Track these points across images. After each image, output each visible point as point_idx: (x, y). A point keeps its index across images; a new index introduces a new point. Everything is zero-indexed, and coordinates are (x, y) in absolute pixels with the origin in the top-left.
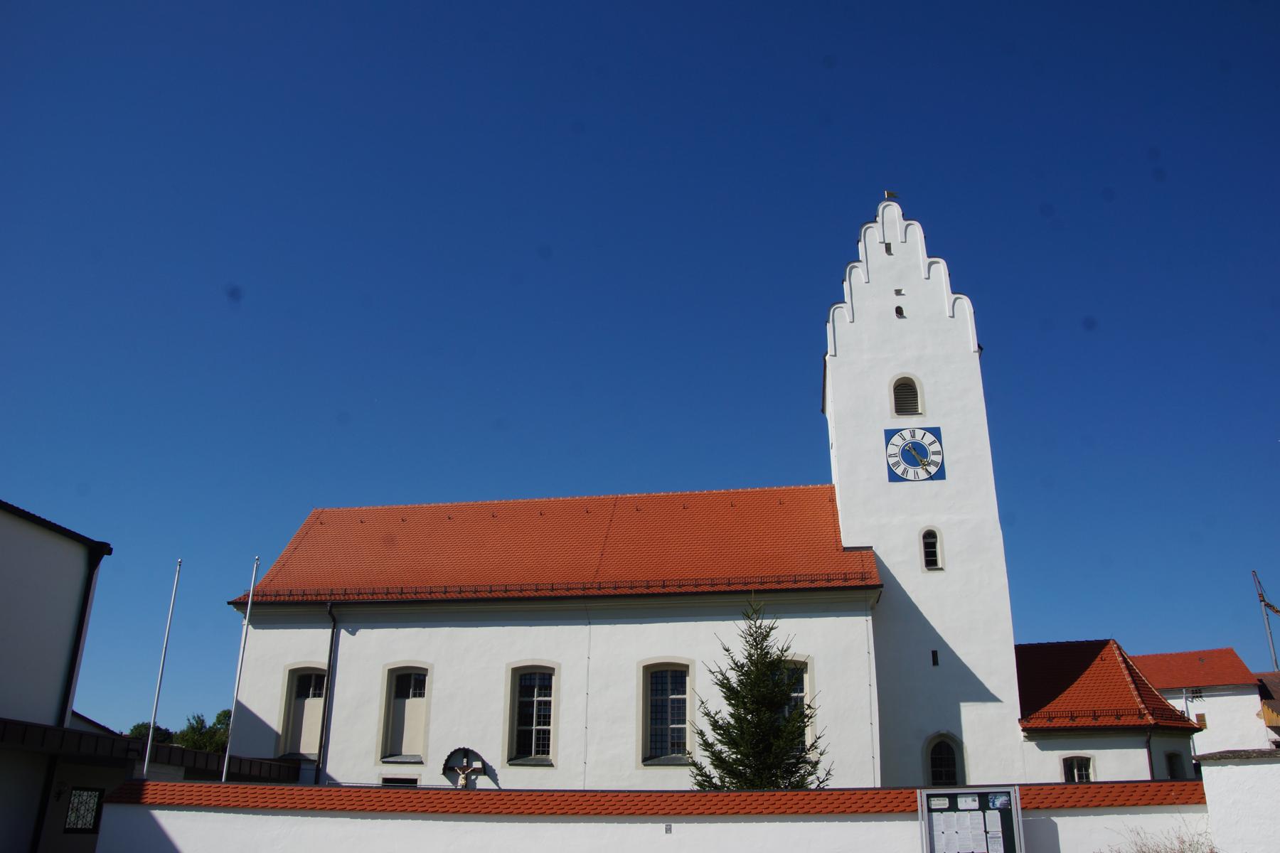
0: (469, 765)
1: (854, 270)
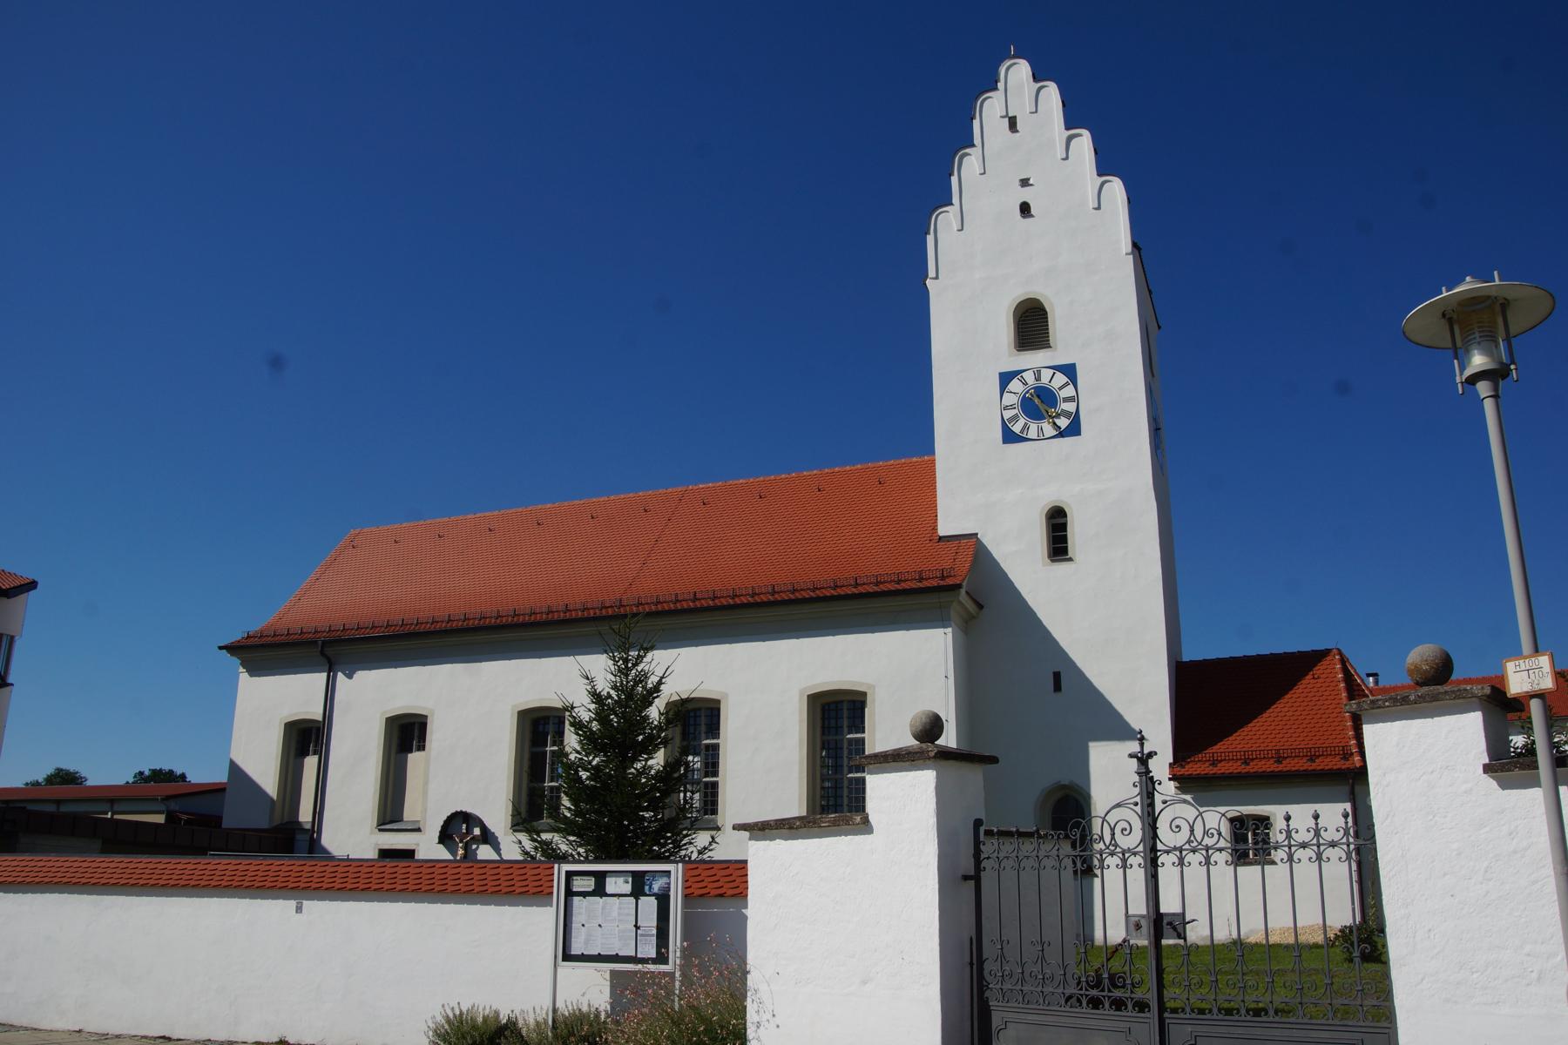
0: (469, 831)
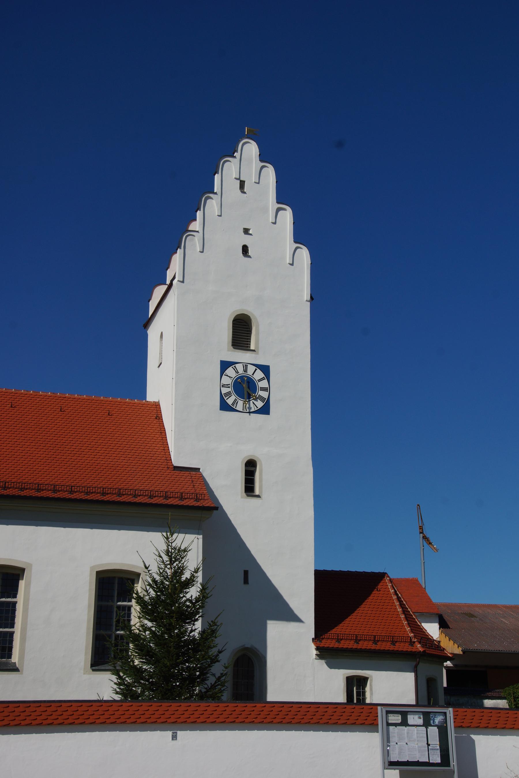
1: (208, 201)
